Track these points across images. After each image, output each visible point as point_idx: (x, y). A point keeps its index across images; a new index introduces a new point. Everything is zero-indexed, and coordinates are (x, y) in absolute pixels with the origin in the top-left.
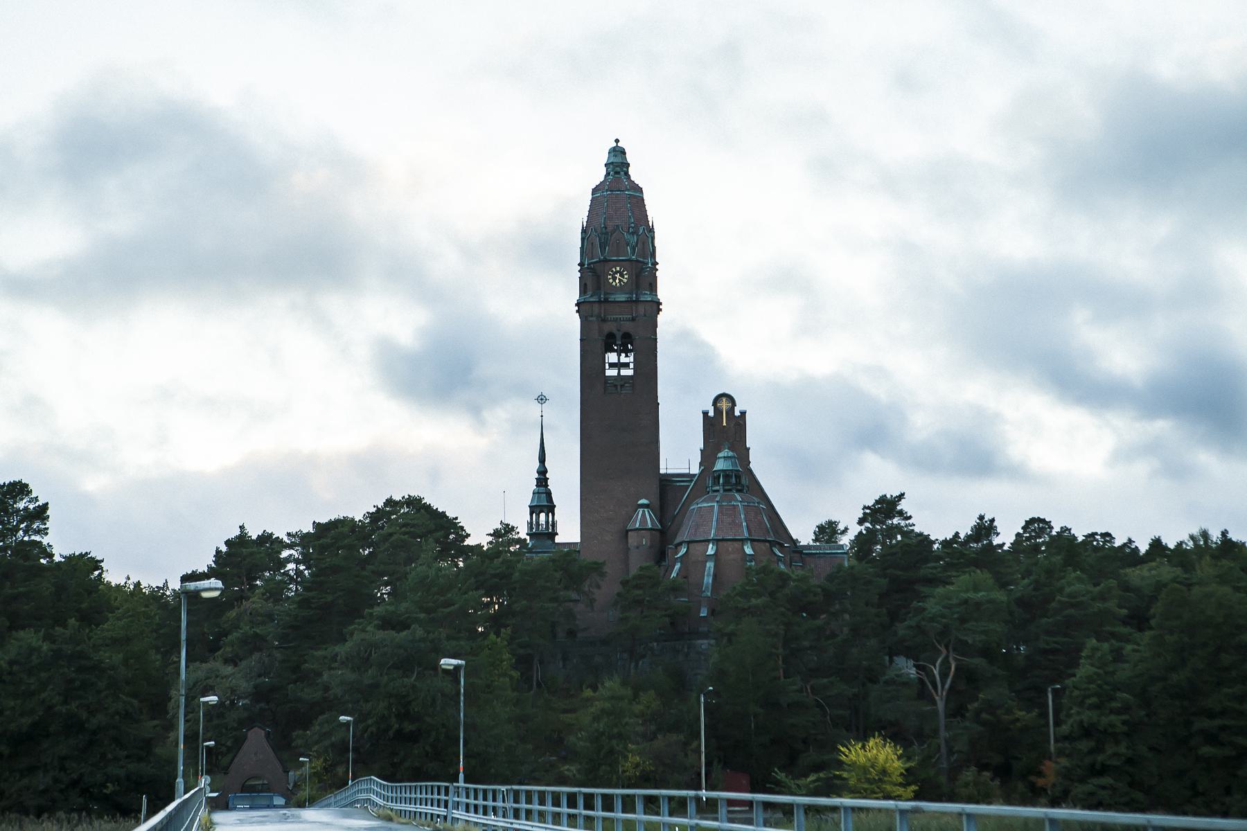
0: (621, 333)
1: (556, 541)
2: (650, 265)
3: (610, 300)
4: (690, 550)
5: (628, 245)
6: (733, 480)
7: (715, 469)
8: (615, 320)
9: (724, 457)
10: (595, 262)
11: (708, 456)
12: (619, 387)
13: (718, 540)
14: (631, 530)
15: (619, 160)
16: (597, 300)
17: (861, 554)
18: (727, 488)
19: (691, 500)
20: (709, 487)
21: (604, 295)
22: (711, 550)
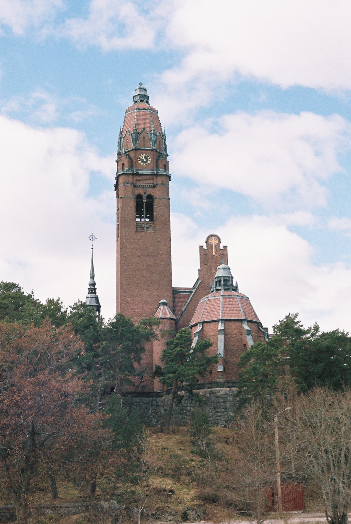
0: (146, 195)
4: (205, 329)
7: (216, 276)
8: (143, 187)
9: (223, 268)
12: (145, 228)
13: (226, 320)
15: (143, 93)
16: (131, 173)
17: (32, 405)
18: (226, 287)
20: (213, 287)
21: (136, 170)
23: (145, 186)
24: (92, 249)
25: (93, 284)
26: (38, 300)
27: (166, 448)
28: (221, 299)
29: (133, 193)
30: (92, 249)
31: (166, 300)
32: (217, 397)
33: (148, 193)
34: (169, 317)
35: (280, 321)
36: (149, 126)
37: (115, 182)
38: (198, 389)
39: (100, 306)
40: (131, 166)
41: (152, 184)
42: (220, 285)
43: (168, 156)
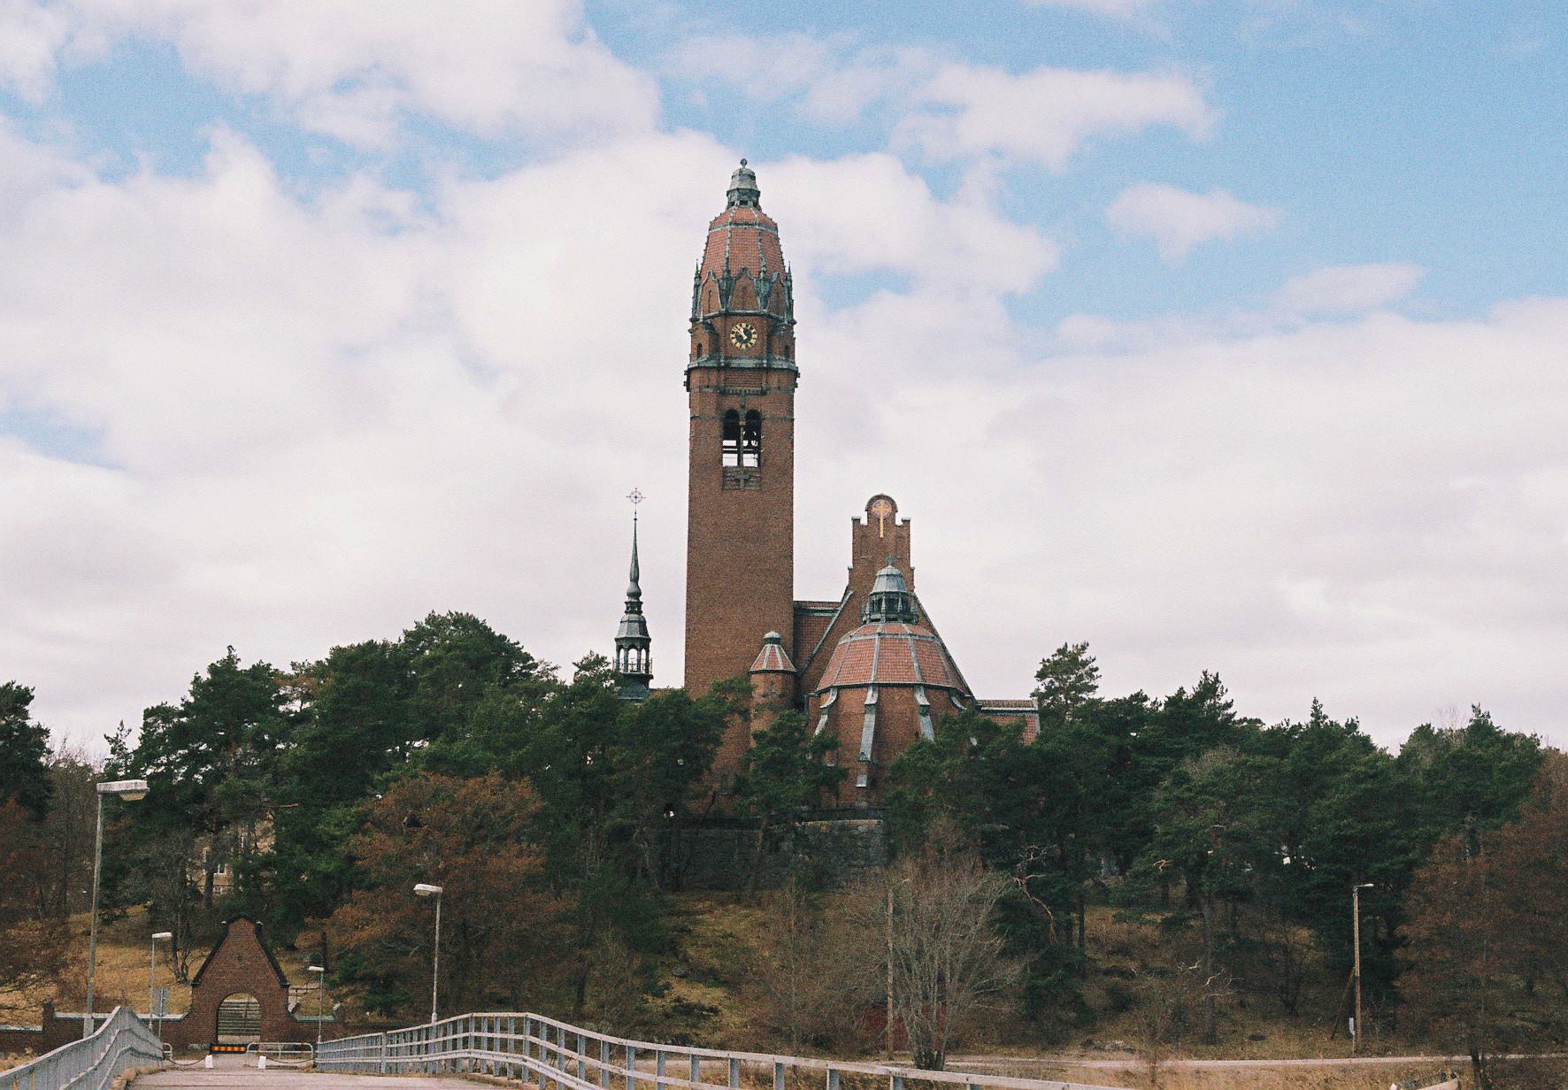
1: (650, 687)
2: (786, 322)
3: (732, 366)
5: (758, 294)
6: (900, 606)
7: (874, 591)
8: (738, 394)
10: (712, 317)
11: (861, 574)
12: (742, 482)
13: (880, 685)
14: (756, 672)
16: (715, 365)
18: (892, 616)
19: (837, 632)
21: (726, 358)
22: (871, 698)
23: (743, 393)
24: (636, 519)
25: (636, 594)
26: (518, 643)
27: (731, 935)
28: (877, 642)
29: (719, 406)
30: (636, 519)
31: (779, 632)
32: (852, 837)
33: (750, 407)
34: (782, 668)
35: (1044, 660)
36: (752, 259)
37: (685, 378)
38: (821, 820)
39: (650, 640)
40: (715, 349)
41: (758, 389)
42: (879, 611)
43: (795, 323)
